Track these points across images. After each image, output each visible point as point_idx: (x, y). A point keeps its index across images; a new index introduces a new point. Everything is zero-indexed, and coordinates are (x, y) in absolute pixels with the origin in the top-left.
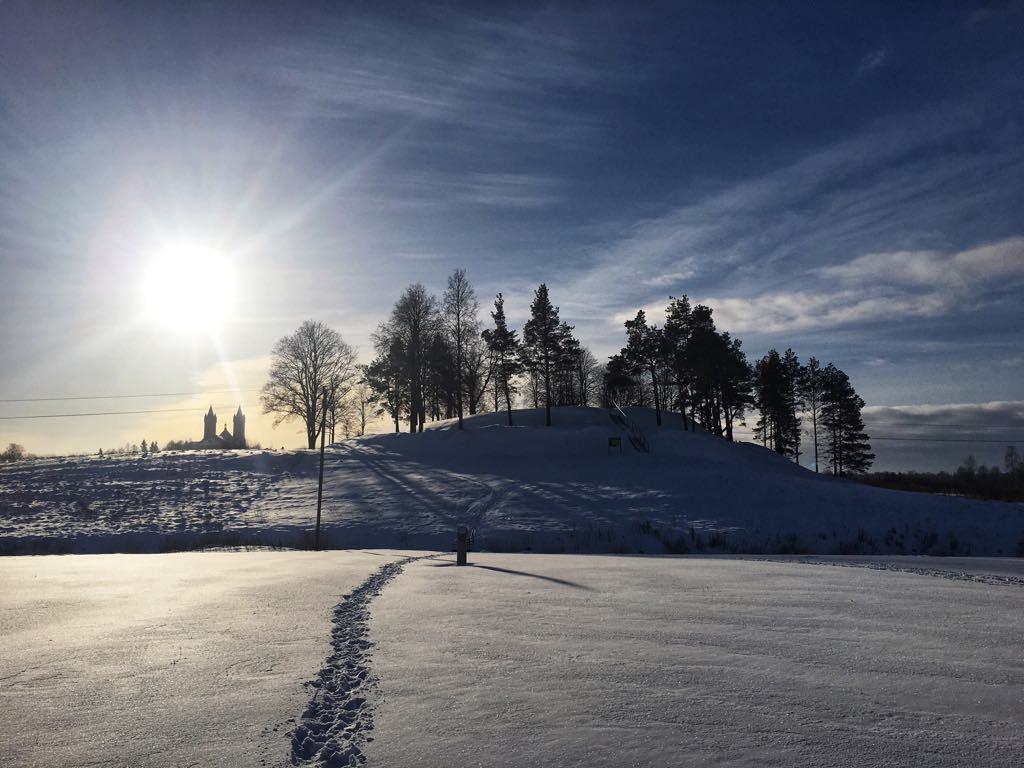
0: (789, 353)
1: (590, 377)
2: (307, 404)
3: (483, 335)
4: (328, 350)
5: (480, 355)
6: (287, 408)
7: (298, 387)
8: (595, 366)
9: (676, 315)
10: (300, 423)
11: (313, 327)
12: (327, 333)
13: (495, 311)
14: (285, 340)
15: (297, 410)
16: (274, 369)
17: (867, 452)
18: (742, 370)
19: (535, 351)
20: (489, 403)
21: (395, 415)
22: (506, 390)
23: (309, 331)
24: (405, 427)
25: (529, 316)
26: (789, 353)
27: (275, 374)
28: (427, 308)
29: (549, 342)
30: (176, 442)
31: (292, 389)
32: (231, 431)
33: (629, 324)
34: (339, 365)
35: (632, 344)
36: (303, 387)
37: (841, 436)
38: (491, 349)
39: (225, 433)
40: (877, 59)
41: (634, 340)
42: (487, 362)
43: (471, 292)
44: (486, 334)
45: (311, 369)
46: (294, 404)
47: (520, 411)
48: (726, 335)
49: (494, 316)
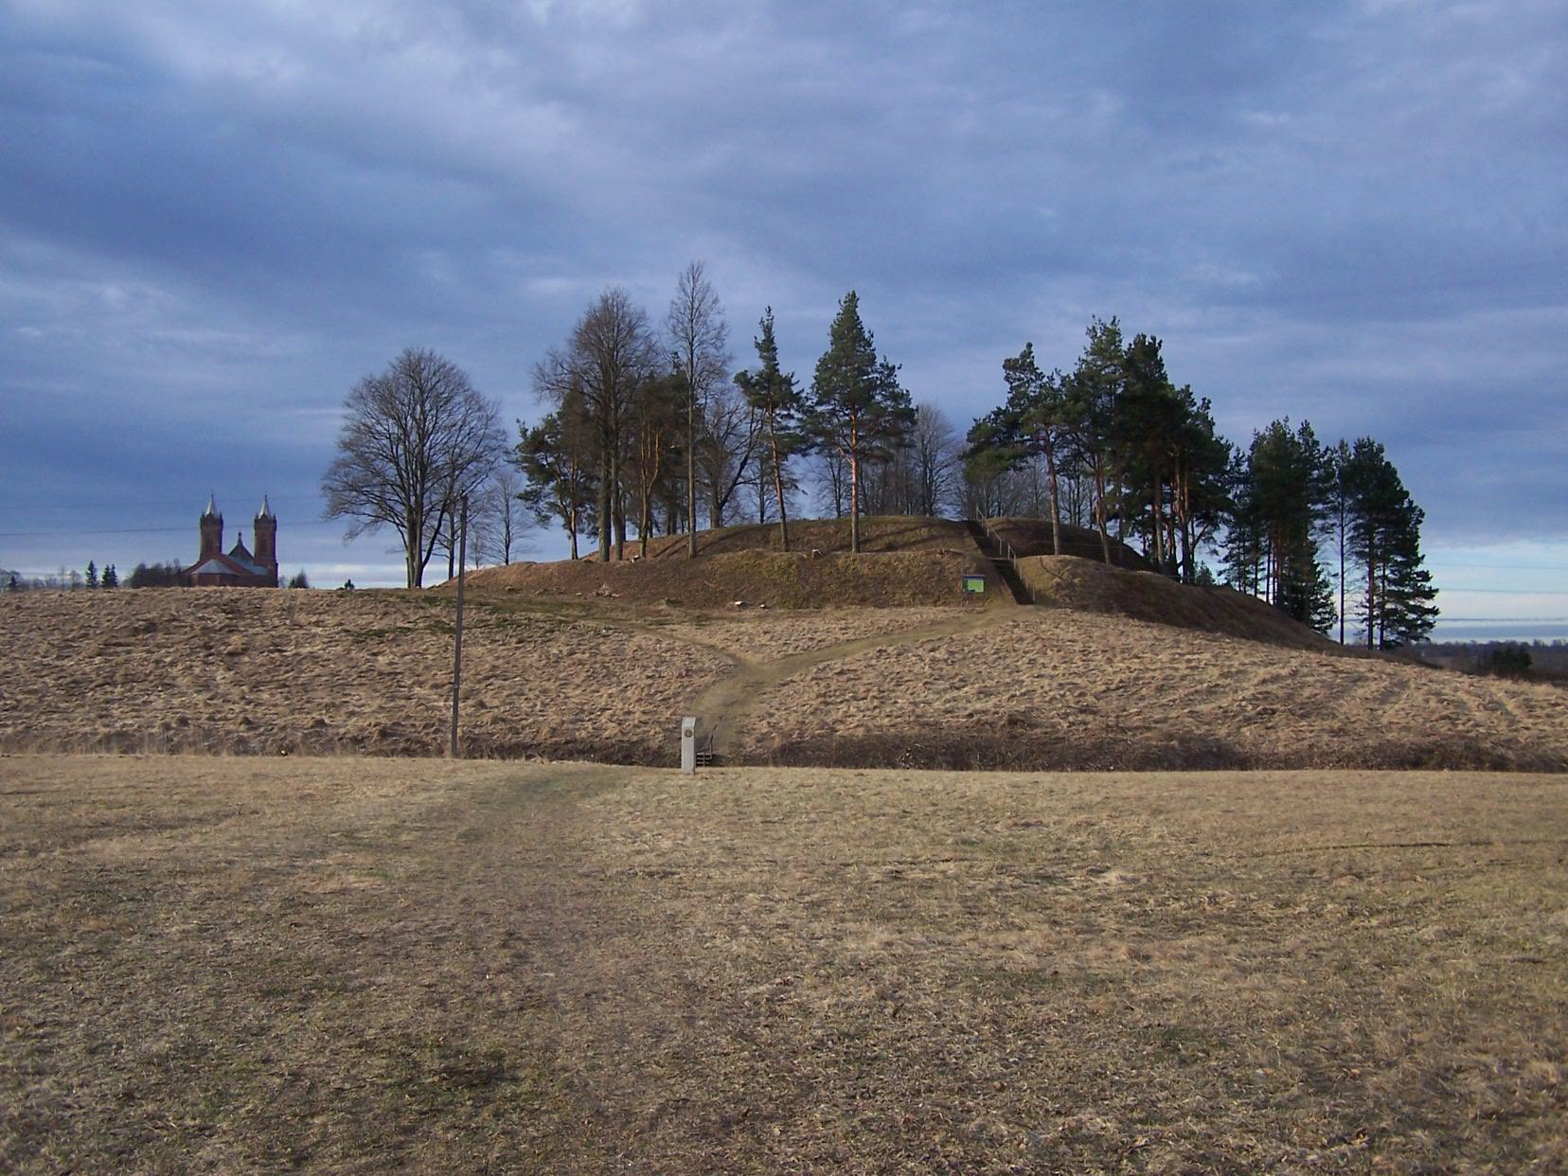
0: (1306, 430)
1: (941, 457)
2: (406, 504)
3: (737, 379)
4: (443, 403)
5: (732, 413)
6: (369, 509)
7: (391, 471)
8: (951, 435)
9: (1098, 351)
10: (392, 536)
11: (420, 358)
12: (445, 372)
13: (761, 337)
14: (369, 384)
15: (386, 513)
16: (347, 435)
17: (1428, 604)
18: (1211, 452)
19: (833, 413)
20: (748, 500)
21: (572, 529)
22: (779, 482)
23: (413, 369)
24: (589, 546)
25: (825, 345)
26: (1306, 430)
27: (347, 446)
28: (631, 328)
29: (859, 398)
30: (149, 566)
31: (377, 474)
32: (251, 547)
33: (1009, 365)
34: (467, 429)
35: (1011, 401)
36: (399, 470)
37: (1384, 577)
38: (753, 404)
39: (240, 549)
40: (34, 332)
41: (1017, 396)
42: (744, 428)
43: (716, 301)
44: (743, 379)
45: (414, 437)
46: (382, 502)
47: (1094, 559)
48: (1187, 392)
49: (757, 345)
